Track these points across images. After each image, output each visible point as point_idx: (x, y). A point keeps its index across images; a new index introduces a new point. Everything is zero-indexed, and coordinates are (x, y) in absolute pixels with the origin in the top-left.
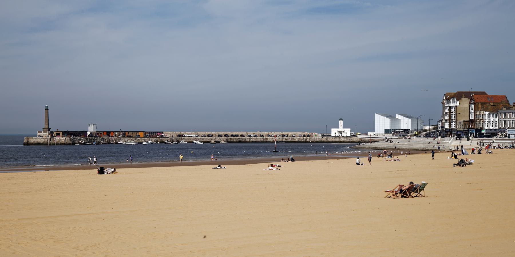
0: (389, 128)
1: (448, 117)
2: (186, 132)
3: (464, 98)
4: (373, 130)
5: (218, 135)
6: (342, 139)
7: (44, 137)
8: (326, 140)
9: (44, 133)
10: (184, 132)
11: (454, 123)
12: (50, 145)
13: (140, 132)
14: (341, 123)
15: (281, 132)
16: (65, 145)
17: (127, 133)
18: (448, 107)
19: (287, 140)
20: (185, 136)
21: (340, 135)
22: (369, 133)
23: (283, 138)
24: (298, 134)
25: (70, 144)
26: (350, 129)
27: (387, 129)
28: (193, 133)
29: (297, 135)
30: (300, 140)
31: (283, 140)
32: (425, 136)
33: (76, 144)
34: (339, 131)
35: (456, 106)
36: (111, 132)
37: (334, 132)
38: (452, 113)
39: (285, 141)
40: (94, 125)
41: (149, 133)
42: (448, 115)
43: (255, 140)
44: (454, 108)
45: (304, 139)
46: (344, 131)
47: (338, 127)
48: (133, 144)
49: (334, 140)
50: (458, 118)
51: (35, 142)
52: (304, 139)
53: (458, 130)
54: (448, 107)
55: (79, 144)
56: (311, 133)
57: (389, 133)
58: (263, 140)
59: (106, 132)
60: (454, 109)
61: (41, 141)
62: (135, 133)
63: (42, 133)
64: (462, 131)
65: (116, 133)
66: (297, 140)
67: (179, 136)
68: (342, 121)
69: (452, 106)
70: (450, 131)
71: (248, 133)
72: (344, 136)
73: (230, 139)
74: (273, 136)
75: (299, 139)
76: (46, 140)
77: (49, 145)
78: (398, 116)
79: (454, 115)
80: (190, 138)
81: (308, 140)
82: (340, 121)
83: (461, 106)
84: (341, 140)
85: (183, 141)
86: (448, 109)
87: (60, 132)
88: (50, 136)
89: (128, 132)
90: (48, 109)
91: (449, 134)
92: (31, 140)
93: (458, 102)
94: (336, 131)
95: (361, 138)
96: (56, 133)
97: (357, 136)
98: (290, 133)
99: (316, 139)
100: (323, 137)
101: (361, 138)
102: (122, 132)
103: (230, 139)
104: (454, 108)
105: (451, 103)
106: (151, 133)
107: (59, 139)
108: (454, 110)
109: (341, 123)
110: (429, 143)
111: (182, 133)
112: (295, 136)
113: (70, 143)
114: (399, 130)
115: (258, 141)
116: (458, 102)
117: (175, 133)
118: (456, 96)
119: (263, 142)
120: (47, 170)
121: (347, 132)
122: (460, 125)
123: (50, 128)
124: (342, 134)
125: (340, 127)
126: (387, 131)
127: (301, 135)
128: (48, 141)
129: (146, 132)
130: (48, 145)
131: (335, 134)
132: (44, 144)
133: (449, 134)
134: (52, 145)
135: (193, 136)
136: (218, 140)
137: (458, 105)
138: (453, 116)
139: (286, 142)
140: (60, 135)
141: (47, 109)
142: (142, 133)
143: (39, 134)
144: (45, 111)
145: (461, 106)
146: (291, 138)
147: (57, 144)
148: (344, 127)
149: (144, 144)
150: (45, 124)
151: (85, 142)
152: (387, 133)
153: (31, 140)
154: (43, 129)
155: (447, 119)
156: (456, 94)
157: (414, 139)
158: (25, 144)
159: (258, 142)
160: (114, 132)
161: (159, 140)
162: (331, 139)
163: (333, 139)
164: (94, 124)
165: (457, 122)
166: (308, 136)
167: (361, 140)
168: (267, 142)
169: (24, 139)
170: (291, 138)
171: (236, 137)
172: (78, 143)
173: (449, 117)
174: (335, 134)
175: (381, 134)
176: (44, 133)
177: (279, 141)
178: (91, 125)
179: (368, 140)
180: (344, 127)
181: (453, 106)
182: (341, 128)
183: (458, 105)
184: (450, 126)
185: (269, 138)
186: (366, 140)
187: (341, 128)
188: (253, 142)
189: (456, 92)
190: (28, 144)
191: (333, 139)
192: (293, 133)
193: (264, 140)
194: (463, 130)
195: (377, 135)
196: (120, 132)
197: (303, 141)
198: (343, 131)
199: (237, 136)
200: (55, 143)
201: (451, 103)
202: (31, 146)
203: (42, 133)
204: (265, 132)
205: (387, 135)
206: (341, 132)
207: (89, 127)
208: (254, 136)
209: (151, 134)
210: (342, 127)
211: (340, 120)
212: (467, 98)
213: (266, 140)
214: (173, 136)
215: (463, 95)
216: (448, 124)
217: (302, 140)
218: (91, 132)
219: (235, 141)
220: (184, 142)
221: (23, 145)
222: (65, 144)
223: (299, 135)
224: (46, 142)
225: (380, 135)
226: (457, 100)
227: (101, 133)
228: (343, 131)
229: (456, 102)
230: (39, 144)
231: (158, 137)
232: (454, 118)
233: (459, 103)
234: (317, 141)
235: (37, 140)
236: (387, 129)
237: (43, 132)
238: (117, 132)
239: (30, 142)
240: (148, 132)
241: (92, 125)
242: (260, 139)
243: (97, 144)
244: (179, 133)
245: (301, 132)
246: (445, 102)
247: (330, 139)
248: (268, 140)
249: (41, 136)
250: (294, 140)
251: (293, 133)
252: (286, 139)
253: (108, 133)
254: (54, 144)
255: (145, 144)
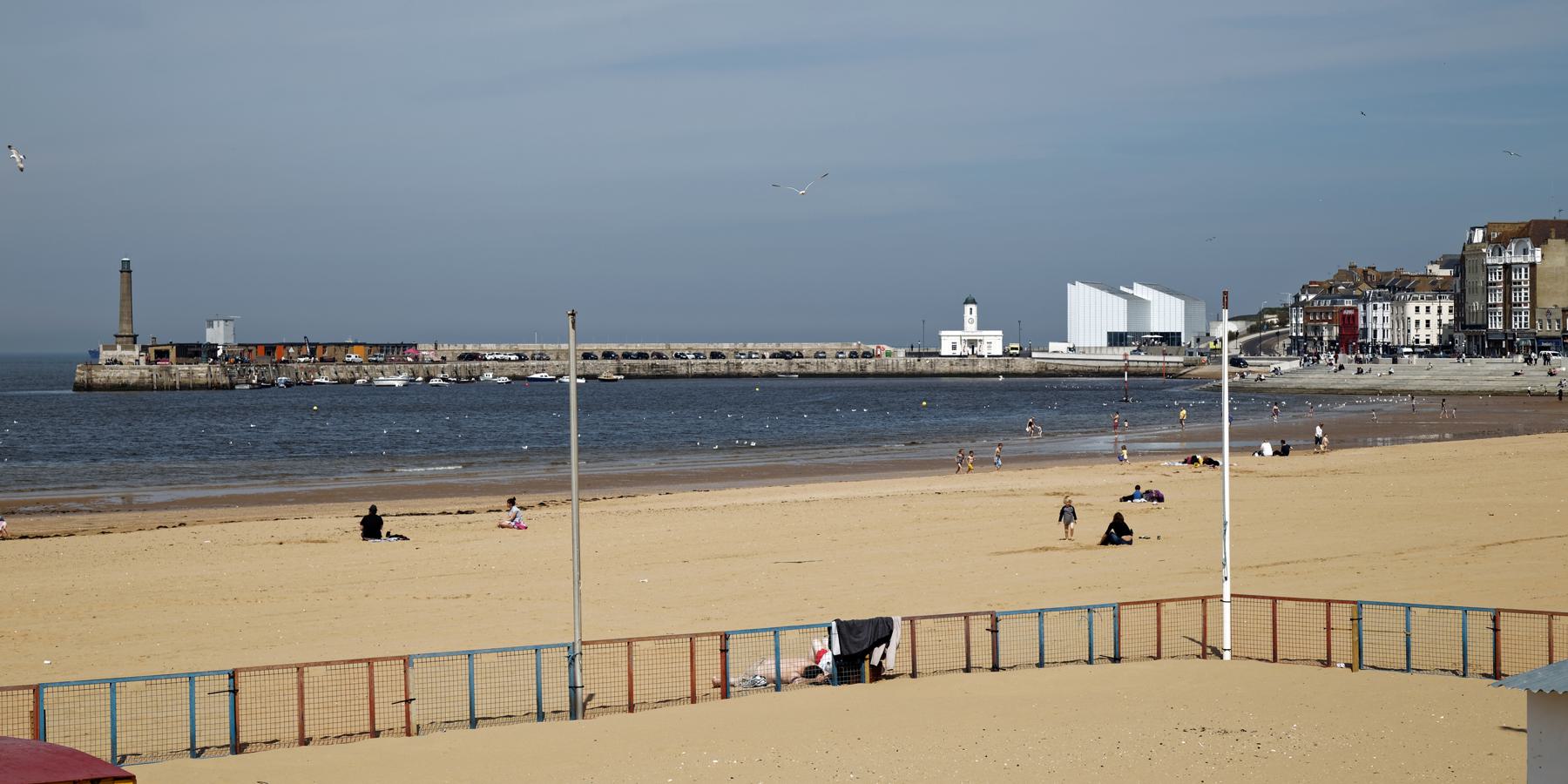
0: (1122, 328)
1: (1500, 295)
2: (483, 345)
3: (1556, 238)
4: (1063, 338)
5: (582, 353)
6: (982, 366)
7: (129, 365)
8: (930, 369)
9: (122, 349)
10: (475, 346)
11: (1523, 316)
12: (161, 388)
13: (355, 347)
14: (970, 314)
15: (774, 344)
16: (208, 389)
17: (320, 349)
18: (1501, 267)
19: (804, 370)
20: (486, 360)
21: (970, 353)
22: (1053, 346)
23: (792, 364)
24: (832, 350)
25: (224, 385)
26: (1000, 333)
27: (1117, 331)
28: (503, 347)
29: (832, 355)
30: (844, 370)
31: (793, 371)
32: (1332, 356)
33: (237, 387)
34: (967, 338)
35: (1533, 265)
36: (278, 347)
37: (950, 342)
38: (1518, 286)
39: (798, 371)
40: (228, 323)
41: (382, 348)
42: (1500, 290)
43: (704, 371)
44: (1523, 270)
45: (857, 366)
46: (981, 338)
47: (961, 328)
48: (397, 384)
49: (956, 369)
50: (1539, 299)
51: (112, 381)
52: (857, 366)
53: (1539, 334)
54: (1501, 267)
55: (248, 387)
56: (874, 347)
57: (1121, 345)
58: (729, 369)
59: (263, 347)
60: (1526, 271)
61: (131, 378)
62: (343, 348)
63: (116, 349)
64: (1558, 338)
65: (291, 350)
66: (834, 369)
67: (466, 360)
68: (974, 307)
69: (1516, 264)
70: (1506, 337)
71: (674, 346)
72: (983, 356)
73: (628, 367)
74: (754, 356)
75: (842, 365)
76: (147, 373)
77: (157, 390)
78: (1140, 290)
79: (1526, 289)
80: (504, 363)
81: (870, 369)
82: (967, 307)
83: (1548, 264)
84: (980, 370)
85: (491, 376)
86: (1500, 273)
87: (169, 348)
88: (142, 360)
89: (325, 346)
90: (130, 272)
91: (1504, 346)
92: (99, 374)
93: (1538, 252)
94: (957, 340)
95: (1046, 361)
96: (156, 352)
97: (1030, 356)
98: (806, 347)
99: (898, 366)
100: (919, 360)
101: (1046, 361)
102: (310, 344)
103: (628, 367)
104: (1523, 270)
105: (1511, 253)
106: (385, 348)
107: (187, 368)
108: (1526, 276)
109: (970, 314)
110: (1517, 374)
111: (470, 348)
112: (825, 357)
113: (224, 382)
114: (1152, 334)
115: (713, 372)
116: (1538, 252)
117: (451, 349)
118: (1530, 233)
119: (728, 376)
120: (1417, 441)
121: (993, 343)
122: (1549, 321)
123: (135, 332)
124: (975, 349)
125: (967, 325)
126: (1173, 339)
127: (842, 353)
128: (155, 377)
129: (371, 346)
130: (153, 389)
131: (954, 348)
132: (142, 387)
133: (1504, 346)
134: (167, 389)
135: (507, 357)
136: (592, 372)
137: (1538, 259)
138: (1523, 294)
139: (802, 376)
140: (168, 357)
141: (126, 269)
142: (362, 347)
143: (104, 352)
144: (122, 277)
145: (1548, 264)
146: (817, 363)
147: (184, 387)
148: (980, 328)
149: (432, 385)
150: (121, 320)
151: (261, 381)
152: (1115, 345)
153: (99, 374)
154: (117, 336)
155: (1498, 302)
156: (1529, 225)
157: (1415, 363)
158: (78, 387)
159: (713, 376)
160: (286, 345)
161: (421, 373)
162: (947, 365)
163: (952, 365)
164: (226, 321)
165: (1537, 310)
166: (867, 355)
167: (1046, 369)
168: (740, 376)
169: (75, 371)
170: (817, 363)
171: (640, 361)
172: (247, 384)
173: (1502, 297)
174: (954, 348)
175: (1096, 348)
176: (122, 349)
177: (779, 373)
178: (215, 323)
179: (1069, 368)
180: (980, 328)
181: (1521, 263)
182: (971, 328)
183: (1538, 259)
184: (1507, 322)
185: (746, 364)
186: (1064, 368)
187: (971, 328)
188: (696, 376)
189: (1528, 221)
190: (89, 387)
191: (952, 365)
192: (818, 346)
193: (732, 370)
194: (1559, 334)
195: (1084, 353)
196: (301, 345)
197: (854, 373)
198: (978, 338)
199: (642, 355)
200: (178, 383)
201: (1511, 253)
202: (97, 392)
203: (116, 349)
204: (724, 344)
205: (1116, 353)
206: (972, 344)
207: (209, 331)
208: (696, 358)
209: (387, 351)
210: (975, 325)
211: (967, 302)
212: (1564, 240)
213: (736, 371)
214: (448, 359)
215: (1553, 230)
216: (1500, 318)
217: (853, 370)
218: (224, 346)
219: (642, 372)
220: (494, 377)
221: (71, 392)
222: (210, 386)
223: (835, 352)
224: (147, 380)
225: (1093, 351)
226: (1536, 244)
227: (250, 348)
228: (980, 340)
229: (1533, 252)
230: (124, 387)
231: (410, 363)
232: (1526, 299)
233: (1543, 256)
234: (900, 370)
235: (118, 375)
236: (1116, 333)
237: (119, 347)
238: (292, 345)
239: (95, 380)
240: (377, 345)
241: (222, 323)
242: (719, 366)
243: (260, 386)
244: (459, 348)
245: (840, 344)
246: (1484, 250)
247: (943, 366)
248: (744, 370)
249: (115, 362)
250: (827, 371)
251: (818, 346)
252: (802, 367)
253: (270, 349)
254: (173, 388)
255: (437, 385)
